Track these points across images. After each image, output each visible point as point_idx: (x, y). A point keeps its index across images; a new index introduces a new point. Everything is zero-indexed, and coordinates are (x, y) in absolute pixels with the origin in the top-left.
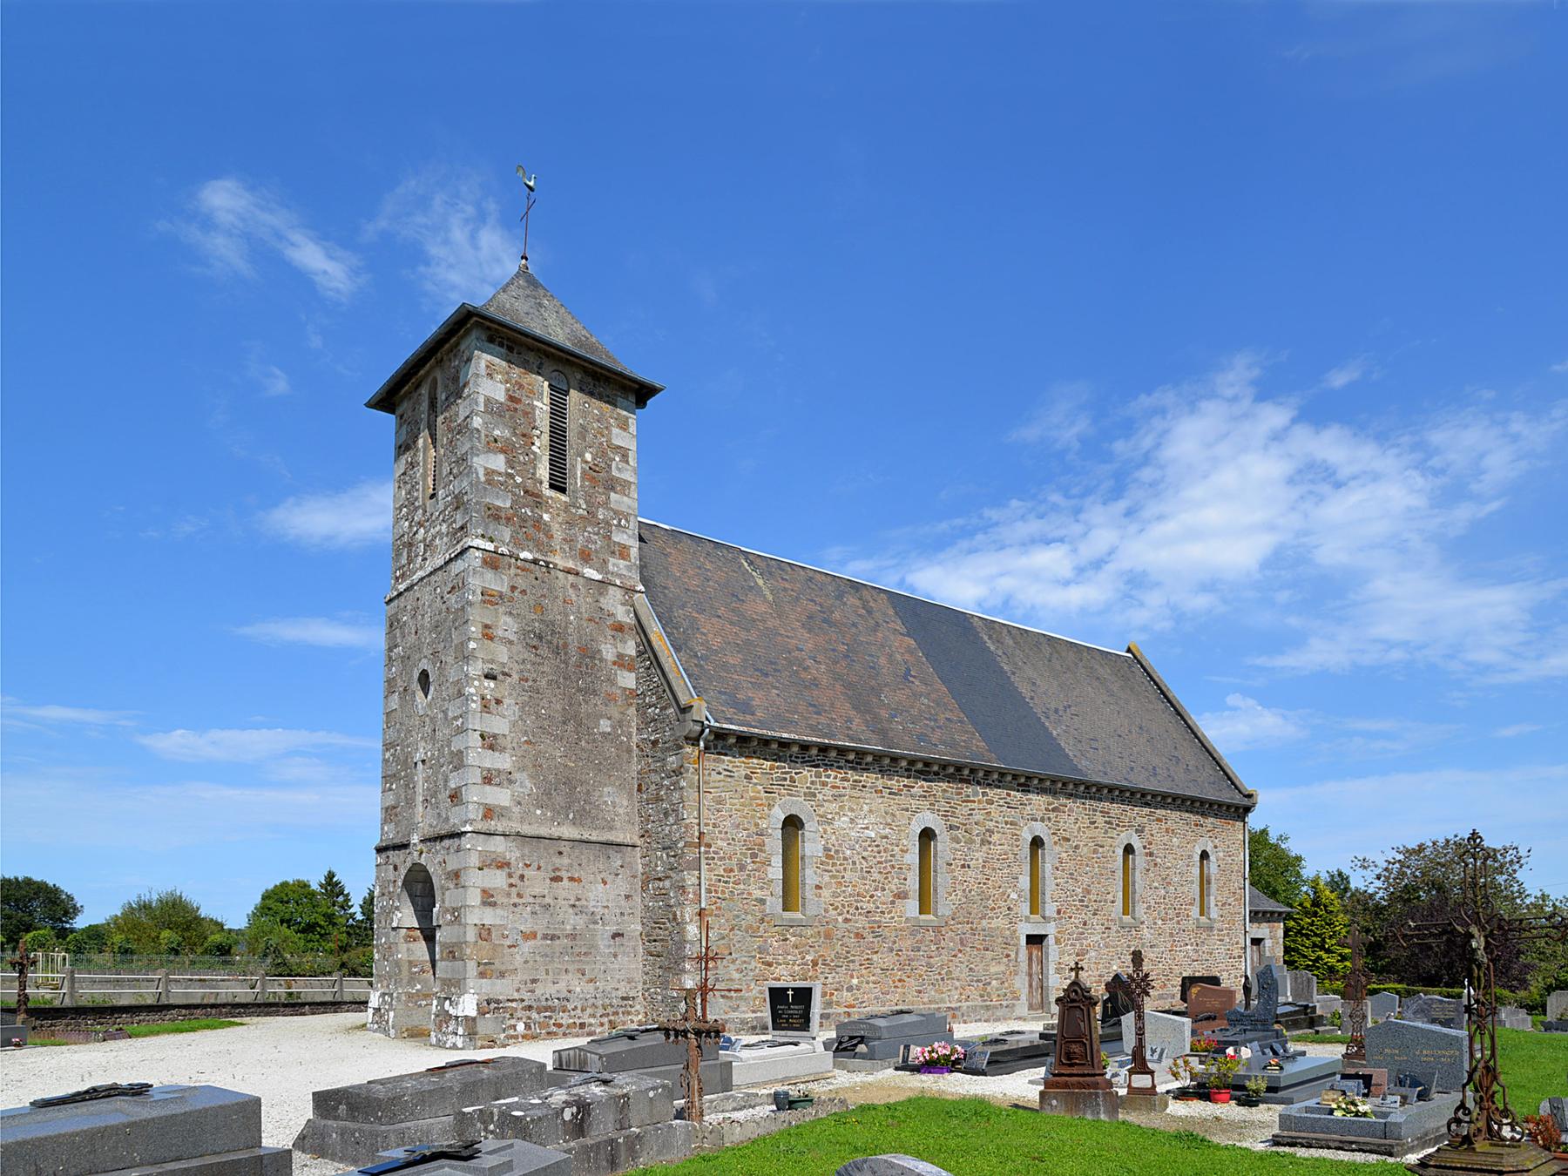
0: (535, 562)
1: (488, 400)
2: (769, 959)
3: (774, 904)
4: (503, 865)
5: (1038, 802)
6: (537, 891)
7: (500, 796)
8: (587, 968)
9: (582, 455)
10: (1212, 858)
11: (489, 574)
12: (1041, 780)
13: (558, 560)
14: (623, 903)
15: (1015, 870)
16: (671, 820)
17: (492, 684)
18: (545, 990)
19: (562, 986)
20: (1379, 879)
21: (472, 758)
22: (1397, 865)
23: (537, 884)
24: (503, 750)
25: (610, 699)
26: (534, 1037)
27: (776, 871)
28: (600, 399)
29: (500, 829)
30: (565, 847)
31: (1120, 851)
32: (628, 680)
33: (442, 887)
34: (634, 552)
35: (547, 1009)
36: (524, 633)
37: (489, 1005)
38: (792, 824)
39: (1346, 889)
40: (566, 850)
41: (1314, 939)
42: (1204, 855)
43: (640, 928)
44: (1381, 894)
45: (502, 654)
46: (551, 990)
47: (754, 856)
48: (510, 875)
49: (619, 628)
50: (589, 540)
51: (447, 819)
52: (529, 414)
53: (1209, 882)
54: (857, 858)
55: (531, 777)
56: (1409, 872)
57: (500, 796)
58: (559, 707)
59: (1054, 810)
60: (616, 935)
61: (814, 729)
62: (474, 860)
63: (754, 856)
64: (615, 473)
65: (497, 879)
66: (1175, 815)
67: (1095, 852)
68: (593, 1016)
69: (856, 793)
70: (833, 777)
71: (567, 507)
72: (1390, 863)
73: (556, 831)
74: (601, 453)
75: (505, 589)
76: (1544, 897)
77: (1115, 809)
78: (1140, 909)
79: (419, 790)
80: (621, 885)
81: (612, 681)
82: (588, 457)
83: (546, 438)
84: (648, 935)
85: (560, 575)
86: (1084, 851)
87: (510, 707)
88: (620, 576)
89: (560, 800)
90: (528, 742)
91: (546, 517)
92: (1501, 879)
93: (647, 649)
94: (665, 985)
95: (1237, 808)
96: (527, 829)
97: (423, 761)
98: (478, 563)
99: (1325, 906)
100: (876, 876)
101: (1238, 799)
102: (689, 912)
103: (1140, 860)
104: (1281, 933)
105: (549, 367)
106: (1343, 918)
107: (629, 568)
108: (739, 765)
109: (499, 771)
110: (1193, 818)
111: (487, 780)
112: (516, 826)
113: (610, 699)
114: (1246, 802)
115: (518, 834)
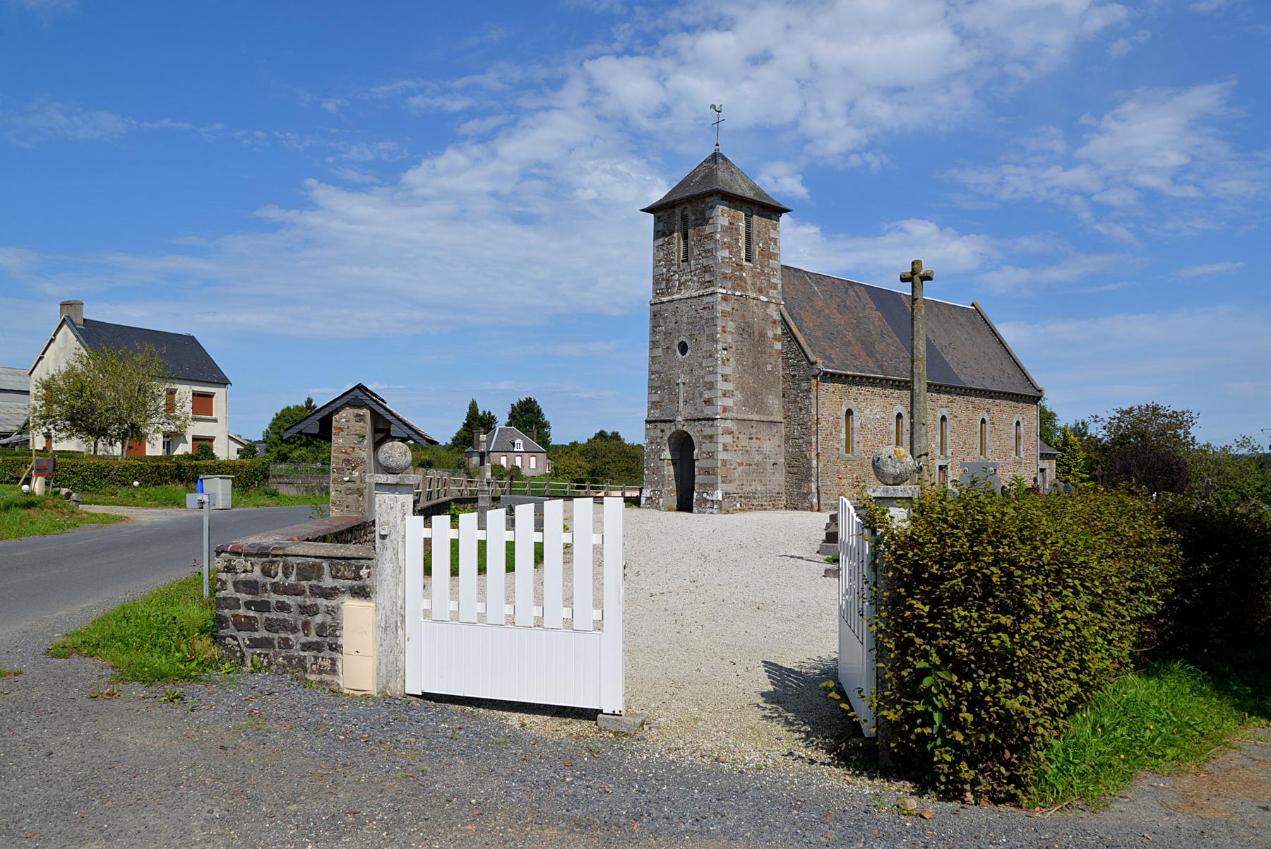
0: (741, 296)
1: (722, 226)
2: (840, 476)
3: (843, 450)
4: (731, 433)
5: (944, 397)
6: (744, 444)
7: (729, 402)
8: (763, 479)
9: (758, 244)
10: (1022, 425)
11: (724, 304)
12: (946, 387)
13: (749, 294)
14: (777, 449)
15: (935, 433)
16: (804, 412)
17: (726, 352)
18: (747, 489)
19: (753, 487)
20: (1105, 429)
21: (719, 386)
22: (1116, 420)
23: (744, 441)
24: (730, 382)
25: (771, 355)
26: (744, 510)
27: (843, 436)
28: (765, 217)
29: (730, 417)
30: (754, 424)
31: (979, 422)
32: (778, 346)
33: (699, 442)
34: (780, 286)
35: (748, 497)
36: (737, 328)
37: (727, 495)
38: (849, 412)
39: (1085, 433)
40: (754, 425)
41: (1064, 467)
42: (1018, 423)
43: (783, 460)
44: (1106, 439)
45: (729, 338)
46: (749, 489)
47: (835, 428)
48: (733, 437)
49: (774, 322)
50: (761, 283)
51: (703, 411)
52: (737, 229)
53: (1020, 438)
54: (872, 428)
55: (741, 393)
56: (1123, 425)
57: (729, 402)
58: (751, 360)
59: (951, 402)
60: (774, 464)
61: (857, 368)
62: (720, 431)
63: (835, 428)
64: (771, 251)
65: (728, 439)
66: (1004, 402)
67: (968, 422)
68: (766, 501)
69: (872, 397)
70: (864, 390)
71: (752, 268)
72: (1111, 419)
73: (750, 417)
74: (766, 243)
75: (730, 310)
76: (1208, 446)
77: (977, 400)
78: (988, 452)
79: (681, 396)
80: (777, 441)
81: (772, 347)
82: (761, 245)
83: (744, 239)
84: (788, 464)
85: (751, 300)
86: (963, 422)
87: (732, 362)
88: (774, 298)
89: (751, 403)
90: (739, 377)
91: (744, 275)
92: (1181, 432)
93: (788, 331)
94: (799, 487)
95: (1034, 397)
96: (740, 417)
97: (684, 384)
98: (719, 299)
99: (1071, 446)
100: (880, 437)
101: (1034, 393)
102: (814, 454)
103: (988, 426)
104: (1054, 466)
105: (745, 207)
106: (1082, 454)
107: (777, 294)
108: (830, 386)
109: (728, 391)
110: (1013, 403)
111: (724, 395)
112: (735, 415)
113: (771, 355)
114: (1038, 394)
115: (737, 419)
